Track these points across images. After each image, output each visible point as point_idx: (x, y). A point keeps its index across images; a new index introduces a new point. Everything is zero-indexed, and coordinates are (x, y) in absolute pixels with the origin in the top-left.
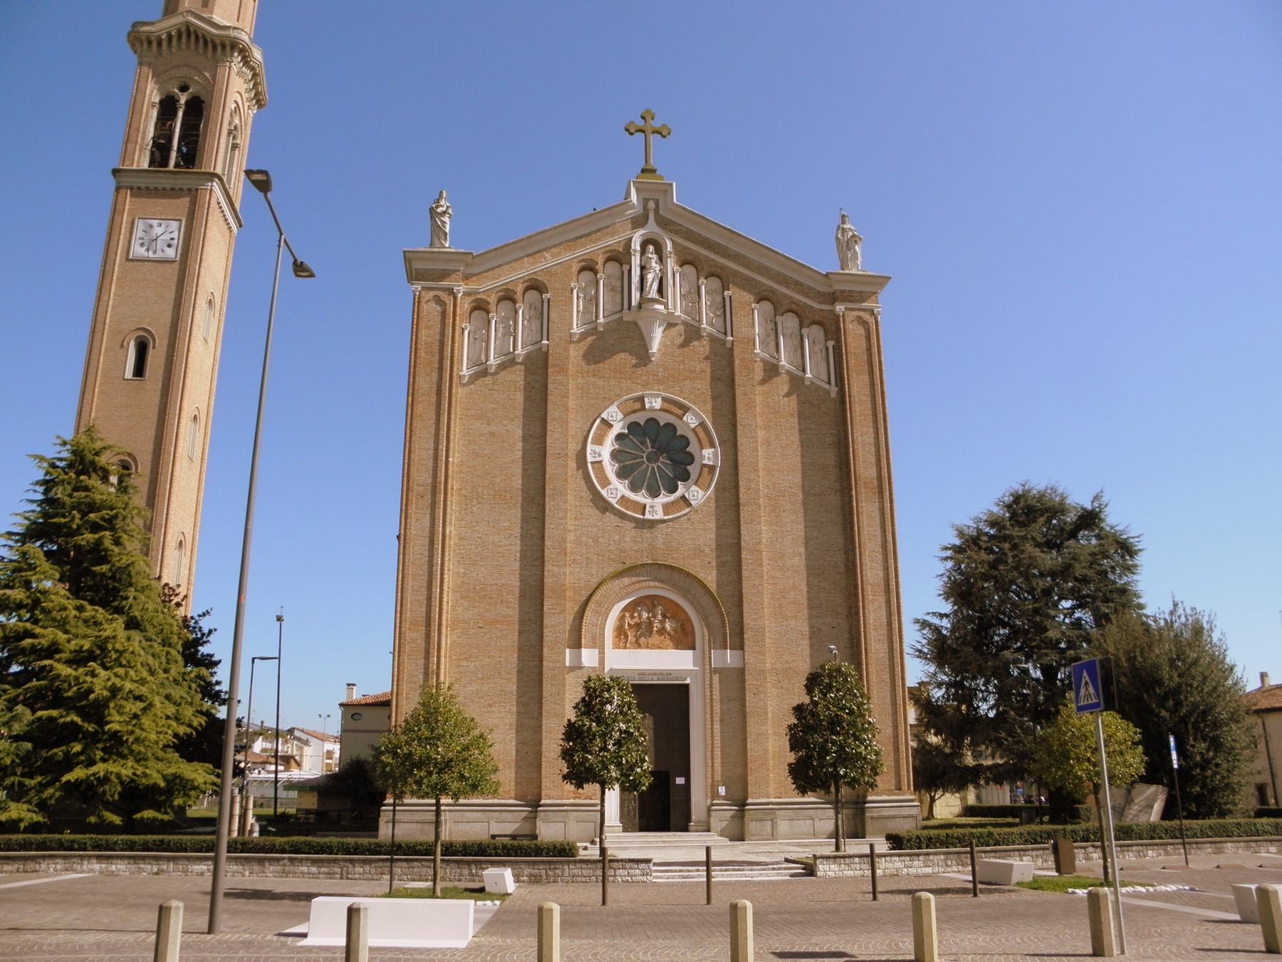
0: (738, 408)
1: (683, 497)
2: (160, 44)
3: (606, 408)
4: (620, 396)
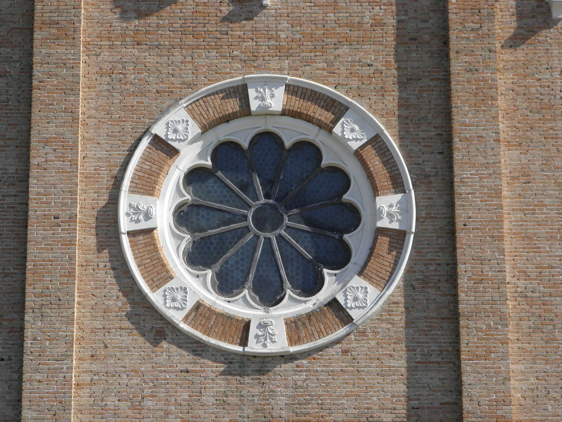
0: (456, 101)
1: (333, 304)
3: (163, 112)
4: (192, 86)
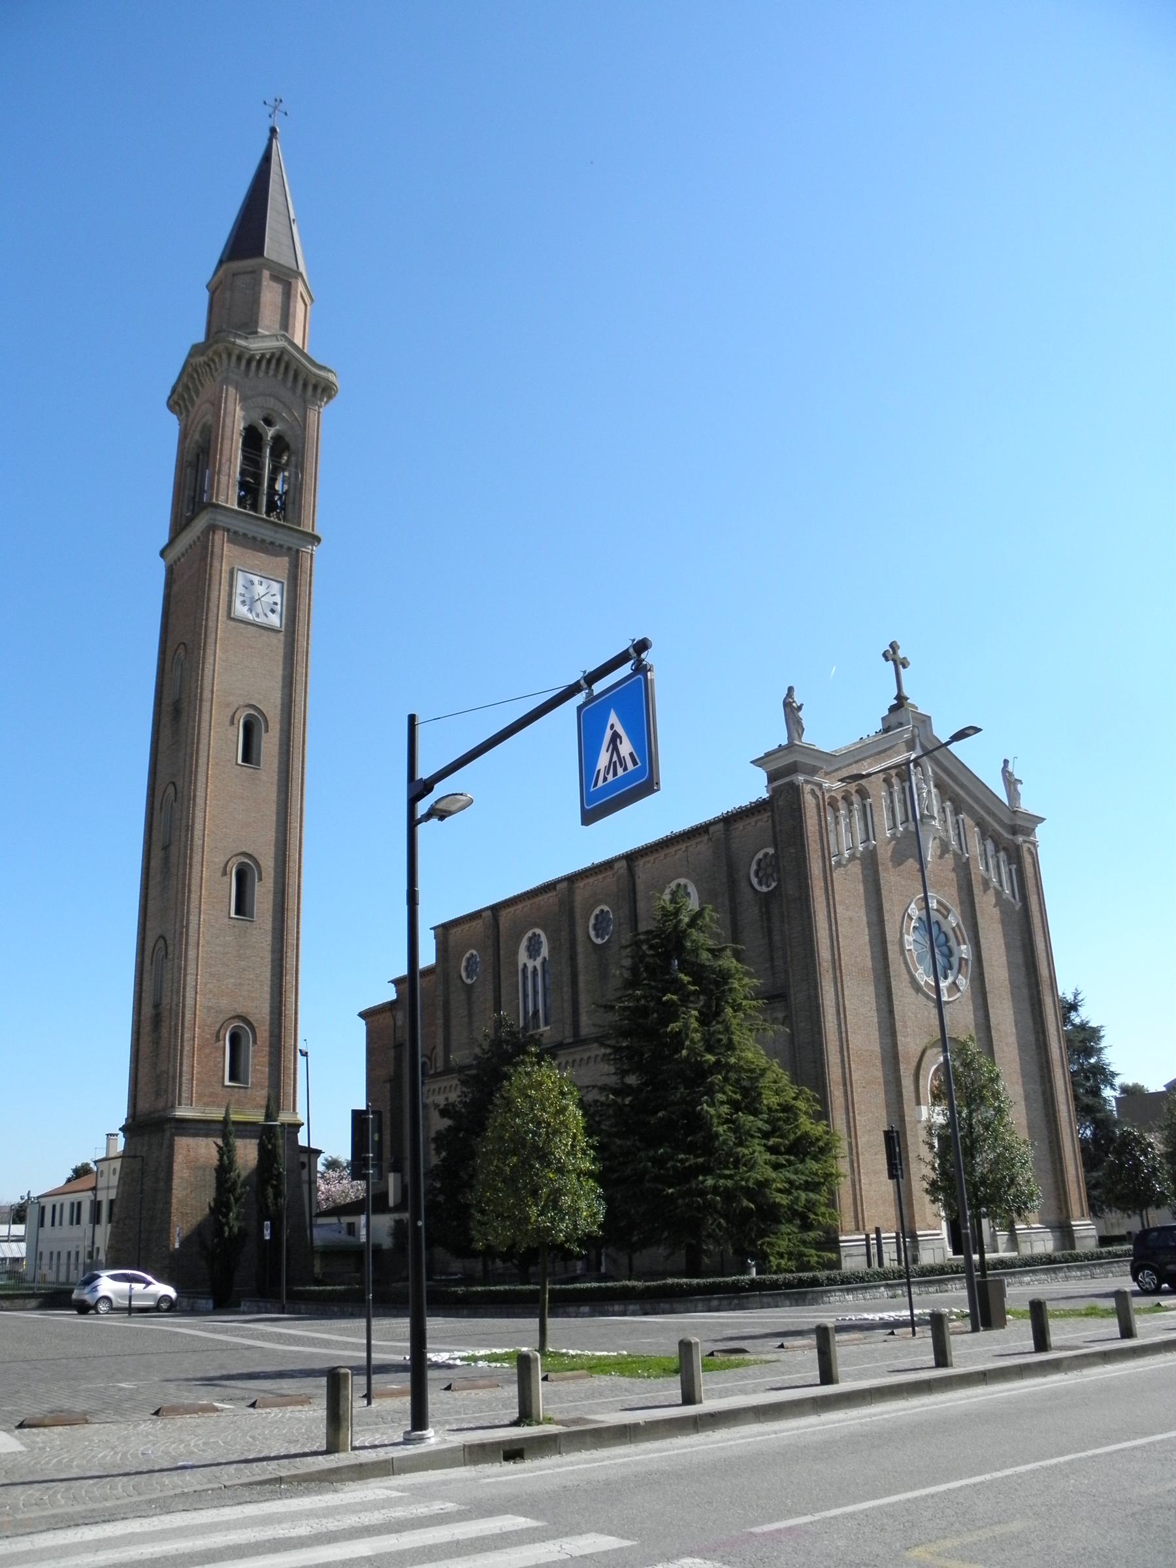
2: (249, 362)
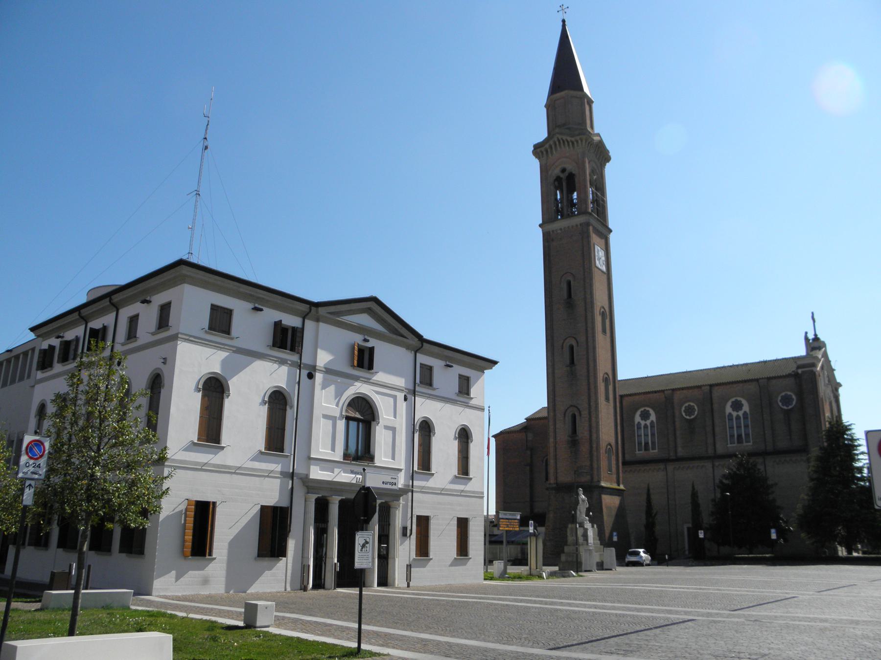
2: (591, 145)
